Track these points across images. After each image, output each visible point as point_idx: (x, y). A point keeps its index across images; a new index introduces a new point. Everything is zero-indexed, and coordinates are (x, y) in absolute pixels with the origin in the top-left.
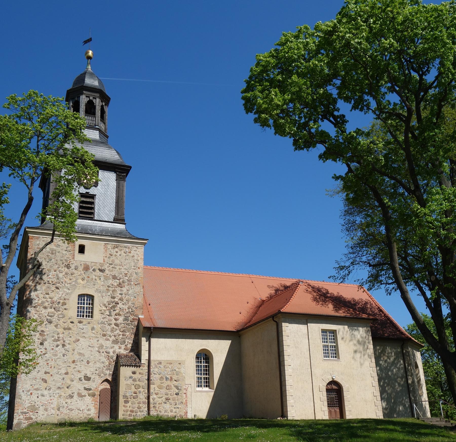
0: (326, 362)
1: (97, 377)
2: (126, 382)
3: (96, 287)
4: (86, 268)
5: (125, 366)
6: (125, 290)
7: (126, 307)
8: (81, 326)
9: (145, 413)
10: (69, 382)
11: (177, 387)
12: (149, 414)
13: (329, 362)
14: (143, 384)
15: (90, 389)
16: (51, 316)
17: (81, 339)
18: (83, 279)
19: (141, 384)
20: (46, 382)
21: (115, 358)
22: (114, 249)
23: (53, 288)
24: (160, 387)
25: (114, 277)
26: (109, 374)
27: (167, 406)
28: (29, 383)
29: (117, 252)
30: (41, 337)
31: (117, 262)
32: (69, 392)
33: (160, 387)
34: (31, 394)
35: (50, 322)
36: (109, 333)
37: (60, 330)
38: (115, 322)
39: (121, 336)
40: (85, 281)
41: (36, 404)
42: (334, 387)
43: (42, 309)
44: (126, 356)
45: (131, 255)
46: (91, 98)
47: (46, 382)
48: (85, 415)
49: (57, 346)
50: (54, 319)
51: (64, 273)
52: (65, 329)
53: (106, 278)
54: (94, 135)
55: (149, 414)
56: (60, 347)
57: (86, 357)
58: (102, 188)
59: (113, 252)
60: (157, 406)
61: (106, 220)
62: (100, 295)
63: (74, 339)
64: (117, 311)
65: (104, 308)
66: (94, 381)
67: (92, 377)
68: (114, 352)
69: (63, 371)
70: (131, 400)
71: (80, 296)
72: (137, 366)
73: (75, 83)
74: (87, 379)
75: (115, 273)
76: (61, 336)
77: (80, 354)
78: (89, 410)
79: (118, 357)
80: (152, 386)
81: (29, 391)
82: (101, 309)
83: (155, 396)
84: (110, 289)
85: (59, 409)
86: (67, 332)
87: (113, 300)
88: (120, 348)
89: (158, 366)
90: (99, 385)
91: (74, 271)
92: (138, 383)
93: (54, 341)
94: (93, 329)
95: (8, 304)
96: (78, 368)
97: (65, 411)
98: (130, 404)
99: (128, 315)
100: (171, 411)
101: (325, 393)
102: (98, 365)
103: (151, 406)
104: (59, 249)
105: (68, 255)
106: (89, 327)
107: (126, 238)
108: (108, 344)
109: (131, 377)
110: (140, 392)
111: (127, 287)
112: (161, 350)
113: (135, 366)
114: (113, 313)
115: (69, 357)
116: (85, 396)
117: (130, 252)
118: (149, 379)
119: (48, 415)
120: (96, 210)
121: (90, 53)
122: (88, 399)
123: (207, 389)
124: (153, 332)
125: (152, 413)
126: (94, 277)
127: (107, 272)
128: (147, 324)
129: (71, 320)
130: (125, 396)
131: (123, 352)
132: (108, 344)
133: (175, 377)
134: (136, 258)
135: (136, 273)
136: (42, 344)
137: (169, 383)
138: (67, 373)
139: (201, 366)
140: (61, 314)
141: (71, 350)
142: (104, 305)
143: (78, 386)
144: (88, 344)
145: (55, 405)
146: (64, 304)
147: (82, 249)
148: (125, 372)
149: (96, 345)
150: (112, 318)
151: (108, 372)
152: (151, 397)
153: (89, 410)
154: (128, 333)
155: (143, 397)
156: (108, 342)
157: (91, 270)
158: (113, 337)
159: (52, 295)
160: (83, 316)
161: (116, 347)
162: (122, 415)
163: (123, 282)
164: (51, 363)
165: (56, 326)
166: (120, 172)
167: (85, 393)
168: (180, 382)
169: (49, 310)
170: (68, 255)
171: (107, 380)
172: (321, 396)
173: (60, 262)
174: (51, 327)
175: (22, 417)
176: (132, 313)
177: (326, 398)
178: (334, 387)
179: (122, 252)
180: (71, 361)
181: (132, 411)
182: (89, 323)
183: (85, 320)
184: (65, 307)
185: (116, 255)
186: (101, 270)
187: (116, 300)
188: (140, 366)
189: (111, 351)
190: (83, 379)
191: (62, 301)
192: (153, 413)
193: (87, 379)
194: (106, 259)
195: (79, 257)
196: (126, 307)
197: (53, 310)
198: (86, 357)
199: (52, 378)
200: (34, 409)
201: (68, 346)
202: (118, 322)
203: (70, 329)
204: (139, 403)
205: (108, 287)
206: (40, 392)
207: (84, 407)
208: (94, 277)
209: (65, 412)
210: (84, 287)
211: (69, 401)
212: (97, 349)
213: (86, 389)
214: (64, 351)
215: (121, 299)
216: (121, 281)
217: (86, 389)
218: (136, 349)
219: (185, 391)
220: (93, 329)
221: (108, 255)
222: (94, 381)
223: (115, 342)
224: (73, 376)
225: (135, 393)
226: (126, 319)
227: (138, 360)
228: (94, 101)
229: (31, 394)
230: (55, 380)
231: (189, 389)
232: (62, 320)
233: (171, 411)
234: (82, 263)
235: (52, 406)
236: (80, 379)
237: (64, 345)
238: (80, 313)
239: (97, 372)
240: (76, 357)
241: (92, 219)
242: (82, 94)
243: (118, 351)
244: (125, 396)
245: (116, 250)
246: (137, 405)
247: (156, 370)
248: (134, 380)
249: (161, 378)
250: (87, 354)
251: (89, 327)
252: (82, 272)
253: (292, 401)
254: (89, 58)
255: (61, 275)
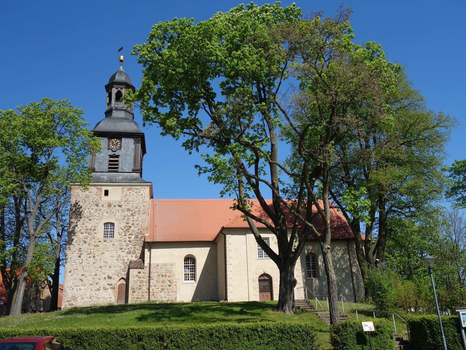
0: (259, 261)
1: (116, 276)
2: (133, 279)
3: (116, 217)
4: (109, 205)
5: (133, 268)
6: (135, 218)
7: (136, 229)
8: (105, 243)
9: (147, 299)
10: (98, 281)
11: (169, 281)
12: (149, 299)
13: (262, 260)
14: (146, 280)
15: (111, 285)
16: (86, 238)
17: (106, 252)
18: (107, 213)
19: (144, 280)
20: (82, 281)
21: (128, 263)
22: (128, 190)
23: (87, 220)
24: (157, 282)
25: (129, 210)
26: (125, 274)
27: (162, 294)
28: (71, 282)
29: (130, 193)
30: (79, 253)
31: (130, 199)
32: (97, 287)
33: (157, 282)
34: (73, 289)
35: (85, 242)
36: (124, 247)
37: (92, 247)
38: (129, 239)
39: (133, 249)
40: (109, 214)
41: (76, 295)
42: (266, 278)
43: (80, 234)
44: (135, 262)
45: (140, 194)
46: (119, 89)
47: (82, 281)
48: (108, 301)
49: (90, 257)
50: (88, 240)
51: (94, 210)
52: (95, 246)
53: (123, 211)
54: (122, 114)
55: (149, 299)
56: (92, 258)
57: (109, 263)
58: (124, 150)
59: (128, 193)
60: (155, 294)
61: (127, 171)
62: (118, 222)
63: (101, 253)
64: (130, 232)
65: (121, 231)
66: (114, 279)
67: (113, 276)
68: (128, 259)
69: (94, 273)
70: (137, 291)
71: (106, 224)
72: (141, 268)
73: (110, 80)
74: (110, 278)
75: (129, 207)
76: (92, 251)
77: (105, 262)
78: (110, 298)
79: (130, 262)
80: (151, 281)
81: (71, 287)
82: (119, 231)
83: (154, 288)
84: (125, 218)
85: (90, 298)
86: (96, 248)
87: (127, 225)
88: (132, 256)
89: (156, 267)
90: (116, 281)
91: (101, 208)
92: (142, 279)
93: (87, 254)
94: (113, 245)
95: (33, 235)
96: (103, 271)
97: (95, 299)
98: (136, 293)
99: (138, 234)
100: (165, 297)
101: (257, 283)
102: (117, 268)
103: (151, 294)
104: (91, 194)
105: (97, 198)
106: (111, 244)
107: (142, 183)
108: (124, 254)
109: (137, 276)
110: (143, 285)
111: (137, 216)
112: (158, 256)
113: (140, 268)
114: (128, 234)
115: (98, 264)
116: (108, 289)
117: (139, 192)
118: (149, 277)
119: (84, 302)
120: (120, 165)
121: (122, 58)
122: (110, 291)
123: (193, 281)
124: (149, 245)
125: (151, 299)
126: (115, 211)
127: (123, 206)
128: (148, 240)
129: (99, 240)
130: (133, 289)
131: (134, 259)
132: (124, 254)
133: (168, 274)
134: (143, 195)
135: (144, 206)
136: (80, 257)
137: (164, 278)
138: (96, 275)
139: (189, 266)
140: (93, 237)
141: (99, 260)
142: (122, 229)
143: (104, 283)
144: (110, 255)
145: (88, 295)
146: (94, 230)
147: (106, 193)
148: (133, 272)
149: (116, 255)
150: (127, 237)
151: (123, 273)
152: (151, 288)
153: (110, 298)
154: (137, 247)
155: (145, 288)
156: (124, 253)
157: (113, 206)
158: (127, 250)
159: (86, 224)
160: (108, 237)
161: (129, 256)
162: (130, 302)
163: (134, 212)
164: (85, 269)
165: (89, 245)
166: (137, 138)
167: (108, 287)
168: (171, 278)
169: (85, 234)
170: (97, 198)
171: (123, 278)
172: (255, 285)
173: (92, 203)
174: (86, 245)
175: (67, 304)
176: (141, 233)
177: (258, 286)
178: (266, 278)
179: (134, 192)
180: (99, 266)
181: (137, 298)
182: (111, 241)
183: (109, 239)
184: (95, 232)
185: (129, 195)
186: (119, 206)
187: (130, 225)
188: (143, 268)
189: (126, 259)
190: (107, 278)
191: (93, 228)
192: (152, 299)
193: (110, 278)
194: (123, 198)
195: (105, 198)
196: (136, 229)
197: (87, 234)
198: (109, 263)
199: (86, 278)
200: (74, 298)
201: (97, 257)
202: (131, 239)
203: (98, 246)
204: (143, 292)
205: (124, 216)
206: (78, 288)
207: (107, 296)
208: (115, 211)
209: (95, 300)
210: (108, 218)
211: (97, 292)
212: (116, 258)
213: (108, 284)
214: (94, 261)
215: (133, 224)
216: (133, 212)
217: (108, 284)
218: (142, 256)
219: (175, 284)
220: (113, 245)
221: (124, 195)
222: (114, 279)
223: (129, 253)
224: (100, 277)
225: (140, 286)
226: (136, 237)
227: (142, 264)
228: (121, 90)
229: (73, 289)
230: (88, 279)
231: (178, 283)
232: (93, 240)
233: (165, 297)
234: (107, 202)
235: (86, 296)
236: (105, 278)
237: (94, 257)
238: (106, 235)
239: (116, 273)
240: (102, 264)
241: (117, 172)
242: (113, 87)
243: (130, 259)
244: (133, 289)
245: (130, 191)
246: (141, 294)
247: (155, 270)
248: (140, 278)
249: (159, 275)
250: (109, 262)
251: (111, 244)
252: (107, 208)
253: (231, 289)
254: (121, 61)
255: (92, 211)
